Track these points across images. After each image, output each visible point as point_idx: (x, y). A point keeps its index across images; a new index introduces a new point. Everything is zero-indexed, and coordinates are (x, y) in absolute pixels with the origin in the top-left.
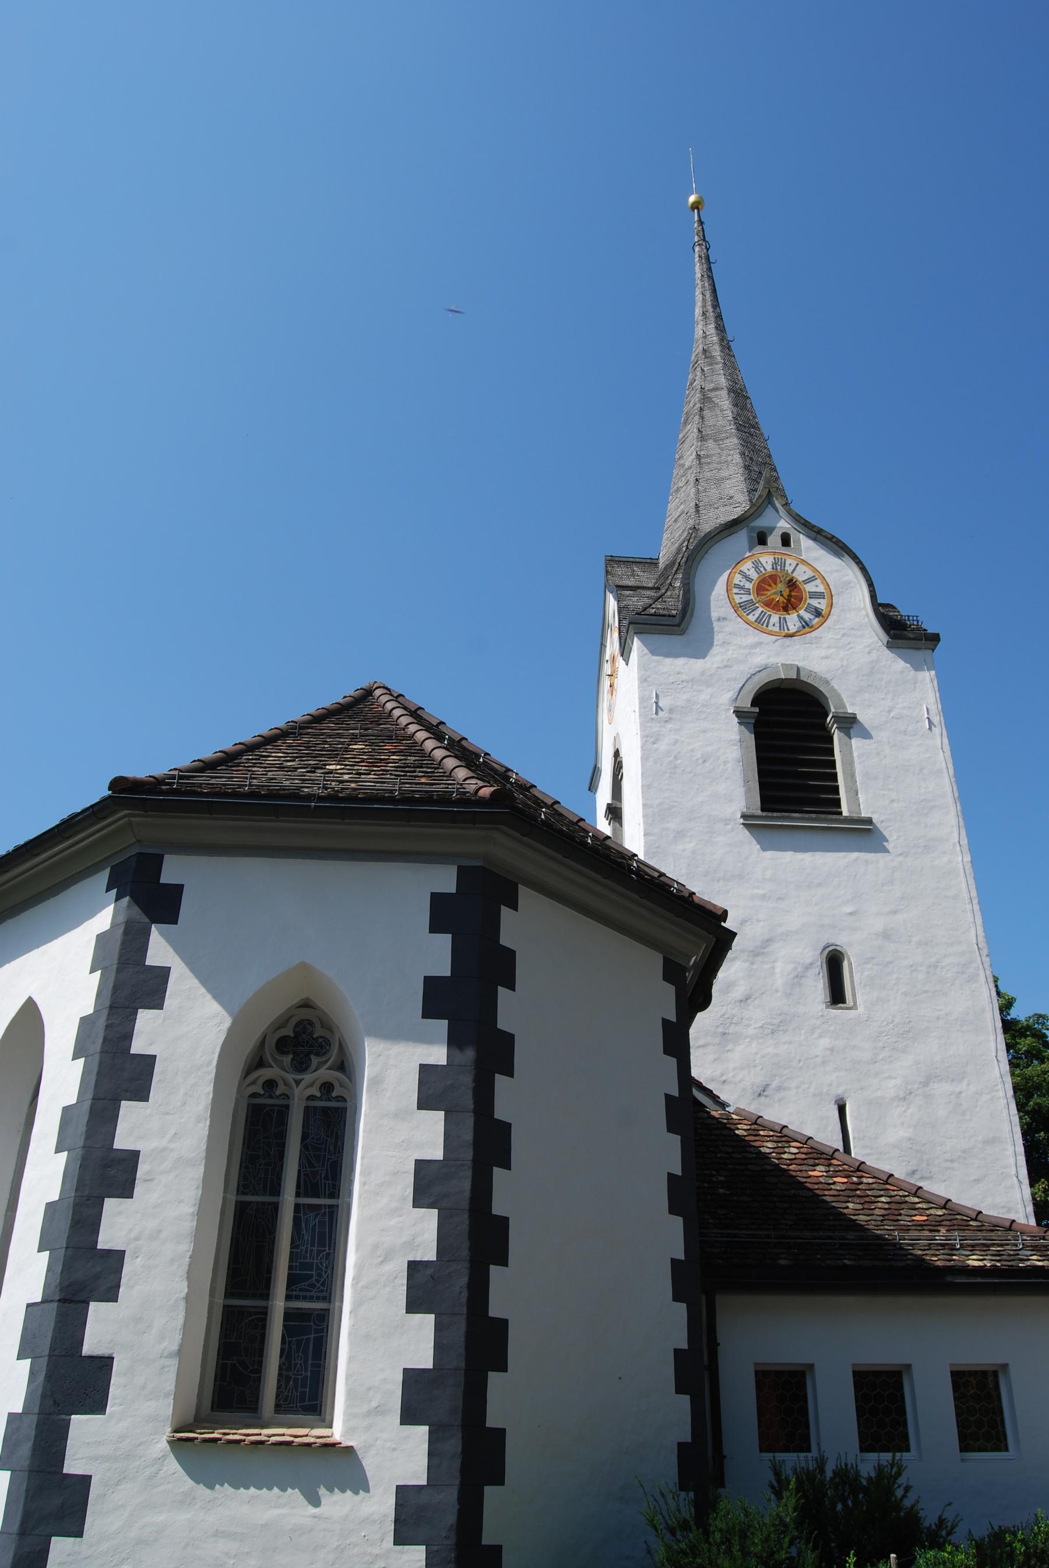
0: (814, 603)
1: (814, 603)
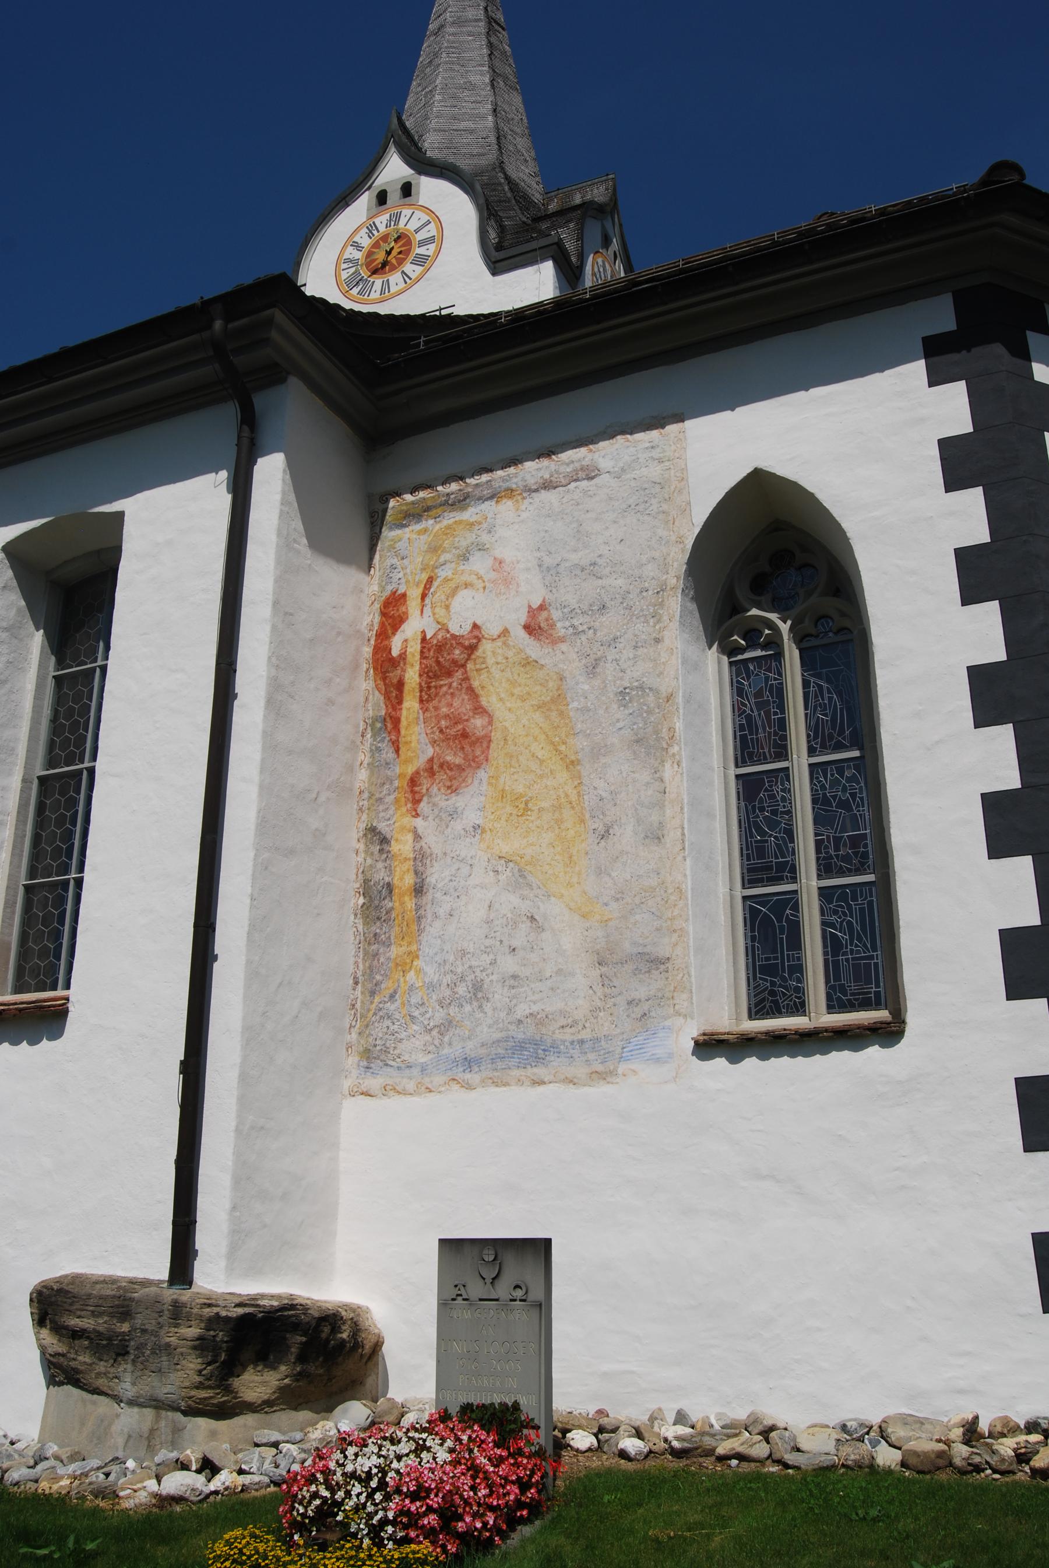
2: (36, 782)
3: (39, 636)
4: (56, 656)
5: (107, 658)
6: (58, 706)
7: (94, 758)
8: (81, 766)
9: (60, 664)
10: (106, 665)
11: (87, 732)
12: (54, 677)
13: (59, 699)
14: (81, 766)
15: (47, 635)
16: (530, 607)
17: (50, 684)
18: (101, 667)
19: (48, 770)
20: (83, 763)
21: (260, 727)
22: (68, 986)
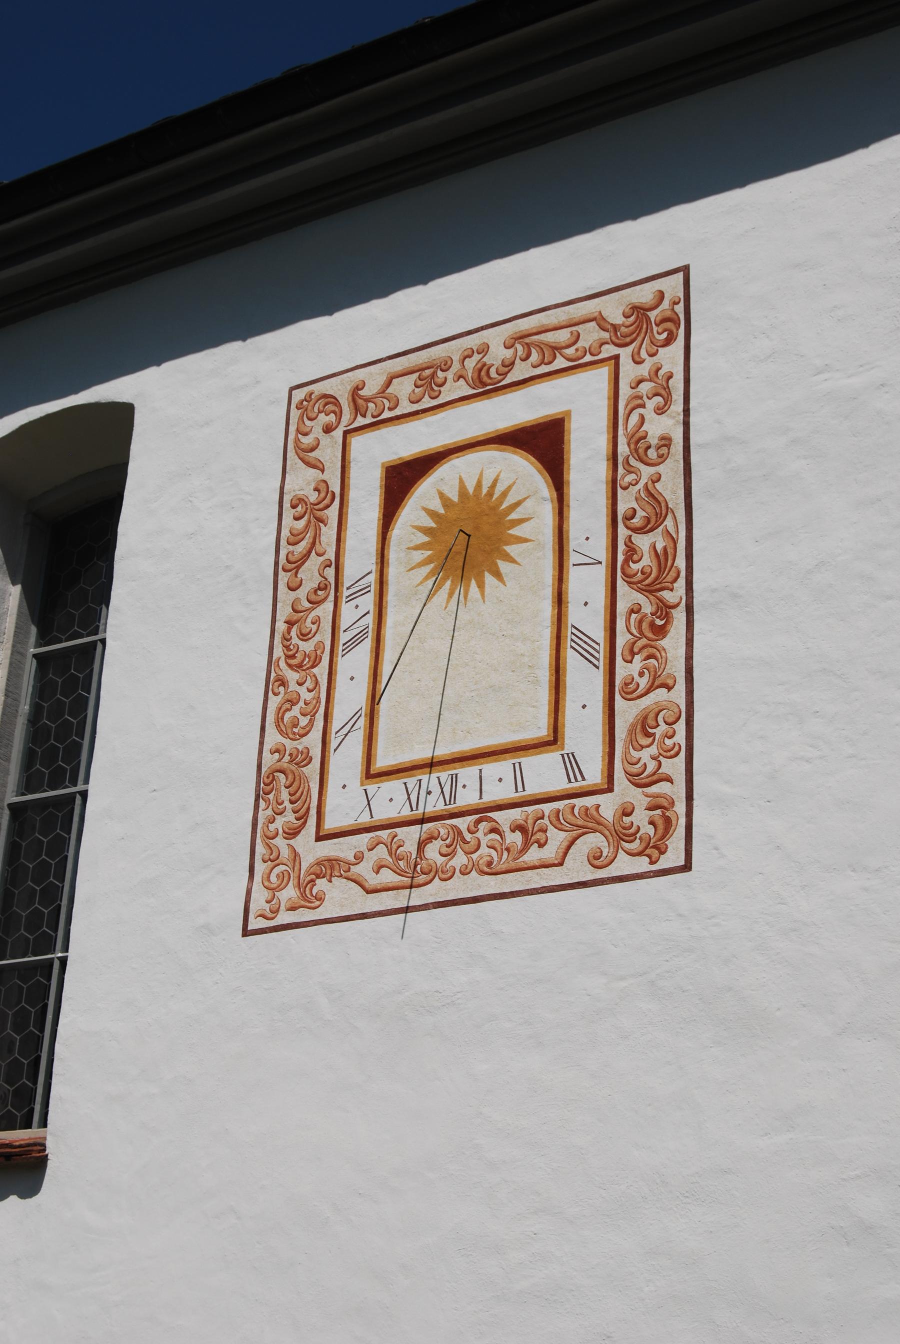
2: (7, 812)
3: (16, 591)
4: (37, 628)
5: (67, 950)
6: (41, 698)
7: (87, 781)
8: (53, 956)
9: (44, 638)
10: (87, 791)
11: (83, 739)
12: (34, 656)
13: (42, 689)
14: (53, 956)
15: (27, 593)
16: (669, 691)
17: (30, 667)
18: (80, 793)
19: (23, 794)
20: (75, 785)
21: (378, 503)
22: (44, 1124)
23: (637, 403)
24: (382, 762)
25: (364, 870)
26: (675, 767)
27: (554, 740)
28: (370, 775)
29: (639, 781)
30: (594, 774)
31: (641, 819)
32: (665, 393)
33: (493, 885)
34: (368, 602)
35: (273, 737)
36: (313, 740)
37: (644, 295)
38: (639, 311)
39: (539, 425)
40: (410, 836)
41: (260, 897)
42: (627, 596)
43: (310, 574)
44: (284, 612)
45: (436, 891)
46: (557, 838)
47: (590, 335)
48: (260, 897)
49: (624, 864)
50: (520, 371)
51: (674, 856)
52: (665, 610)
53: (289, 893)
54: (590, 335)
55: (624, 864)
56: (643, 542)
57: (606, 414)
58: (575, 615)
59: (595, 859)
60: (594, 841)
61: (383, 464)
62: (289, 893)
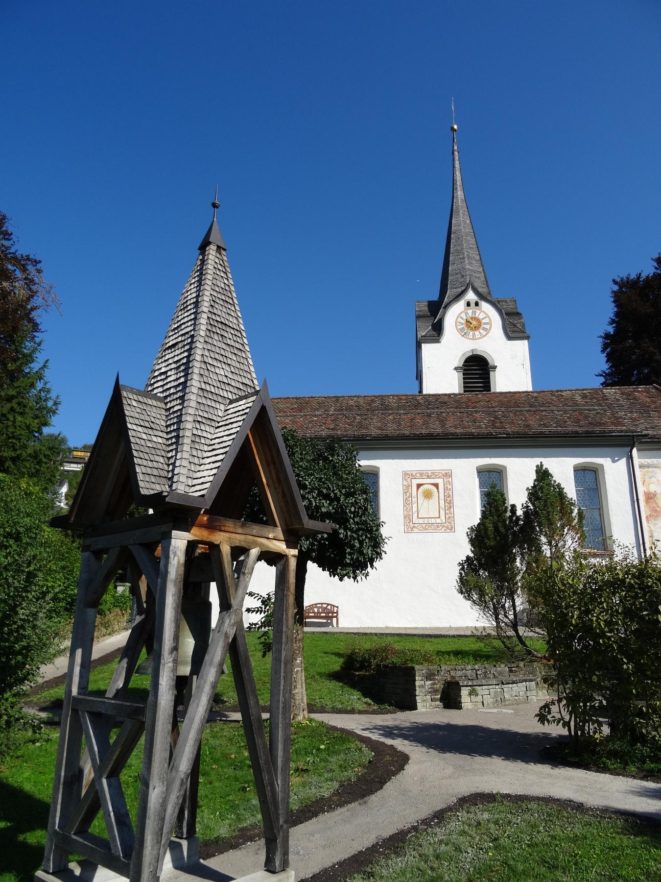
0: (485, 326)
1: (485, 326)
23: (447, 484)
24: (419, 517)
25: (419, 528)
26: (453, 522)
27: (439, 517)
28: (418, 518)
29: (449, 523)
30: (444, 522)
31: (449, 527)
32: (449, 483)
33: (434, 531)
34: (416, 499)
35: (405, 512)
36: (411, 513)
37: (447, 472)
38: (446, 473)
39: (163, 630)
40: (424, 525)
41: (406, 529)
42: (446, 504)
43: (408, 494)
44: (405, 498)
45: (427, 531)
46: (441, 527)
47: (441, 475)
48: (406, 529)
49: (448, 531)
50: (432, 477)
51: (453, 531)
52: (451, 506)
53: (410, 529)
54: (441, 475)
55: (448, 531)
56: (448, 499)
57: (420, 625)
58: (441, 505)
59: (445, 530)
60: (444, 528)
61: (505, 468)
62: (410, 529)
